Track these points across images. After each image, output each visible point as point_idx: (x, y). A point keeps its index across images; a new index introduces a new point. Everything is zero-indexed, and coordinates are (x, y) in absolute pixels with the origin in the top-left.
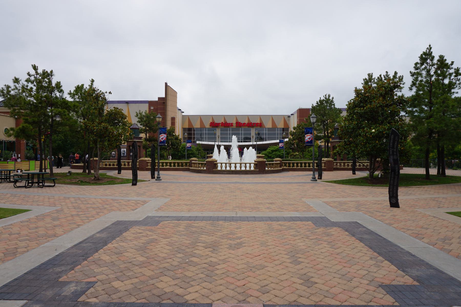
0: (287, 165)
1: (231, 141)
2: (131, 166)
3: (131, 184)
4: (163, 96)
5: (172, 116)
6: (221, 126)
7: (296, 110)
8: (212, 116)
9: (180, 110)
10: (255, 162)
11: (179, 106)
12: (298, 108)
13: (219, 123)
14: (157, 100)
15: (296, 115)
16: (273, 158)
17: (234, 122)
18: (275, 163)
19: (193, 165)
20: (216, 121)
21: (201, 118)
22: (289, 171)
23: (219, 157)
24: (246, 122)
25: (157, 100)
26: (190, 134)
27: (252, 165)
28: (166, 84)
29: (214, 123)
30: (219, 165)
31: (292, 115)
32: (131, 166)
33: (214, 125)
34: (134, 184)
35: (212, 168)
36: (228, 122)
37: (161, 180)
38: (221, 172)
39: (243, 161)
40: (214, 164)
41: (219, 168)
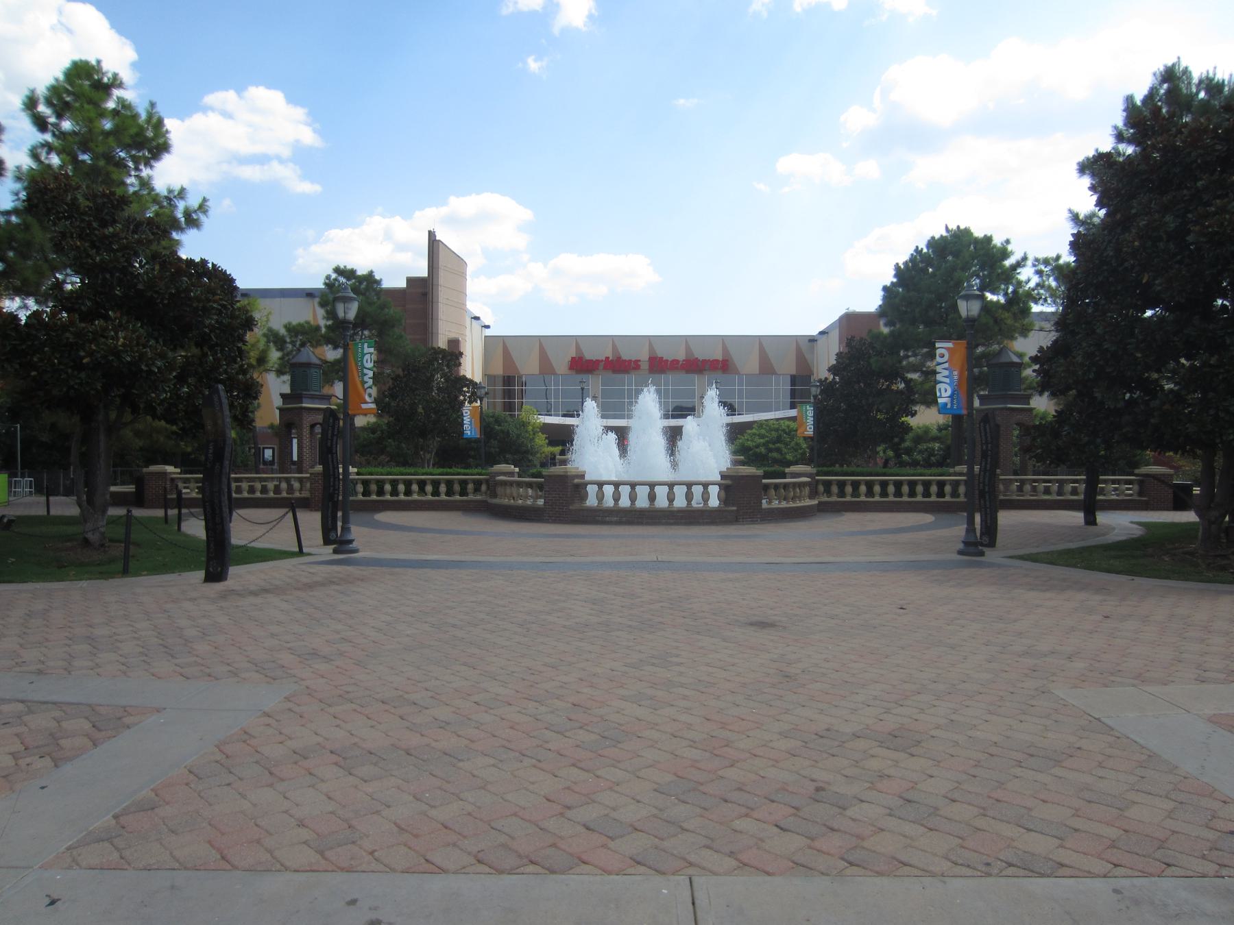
0: (835, 489)
1: (630, 417)
2: (962, 499)
3: (201, 574)
4: (424, 273)
5: (453, 336)
6: (605, 368)
7: (835, 317)
8: (577, 339)
9: (477, 318)
10: (723, 476)
11: (473, 307)
12: (842, 312)
13: (598, 362)
14: (403, 284)
15: (835, 336)
16: (789, 464)
17: (644, 356)
18: (794, 484)
19: (499, 490)
20: (589, 355)
21: (542, 344)
22: (898, 510)
23: (595, 457)
24: (681, 356)
25: (403, 284)
26: (509, 394)
27: (714, 491)
28: (431, 235)
29: (581, 358)
30: (592, 490)
31: (822, 333)
32: (962, 499)
33: (582, 365)
34: (215, 575)
35: (564, 501)
36: (625, 357)
37: (356, 551)
38: (601, 517)
39: (685, 474)
40: (575, 486)
41: (592, 501)
